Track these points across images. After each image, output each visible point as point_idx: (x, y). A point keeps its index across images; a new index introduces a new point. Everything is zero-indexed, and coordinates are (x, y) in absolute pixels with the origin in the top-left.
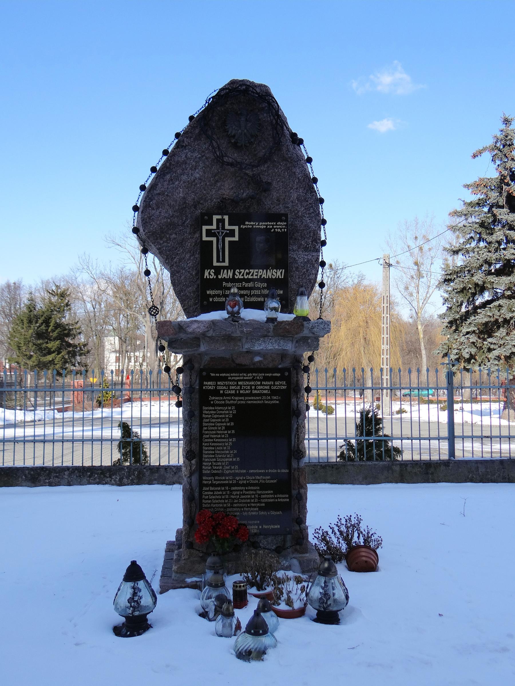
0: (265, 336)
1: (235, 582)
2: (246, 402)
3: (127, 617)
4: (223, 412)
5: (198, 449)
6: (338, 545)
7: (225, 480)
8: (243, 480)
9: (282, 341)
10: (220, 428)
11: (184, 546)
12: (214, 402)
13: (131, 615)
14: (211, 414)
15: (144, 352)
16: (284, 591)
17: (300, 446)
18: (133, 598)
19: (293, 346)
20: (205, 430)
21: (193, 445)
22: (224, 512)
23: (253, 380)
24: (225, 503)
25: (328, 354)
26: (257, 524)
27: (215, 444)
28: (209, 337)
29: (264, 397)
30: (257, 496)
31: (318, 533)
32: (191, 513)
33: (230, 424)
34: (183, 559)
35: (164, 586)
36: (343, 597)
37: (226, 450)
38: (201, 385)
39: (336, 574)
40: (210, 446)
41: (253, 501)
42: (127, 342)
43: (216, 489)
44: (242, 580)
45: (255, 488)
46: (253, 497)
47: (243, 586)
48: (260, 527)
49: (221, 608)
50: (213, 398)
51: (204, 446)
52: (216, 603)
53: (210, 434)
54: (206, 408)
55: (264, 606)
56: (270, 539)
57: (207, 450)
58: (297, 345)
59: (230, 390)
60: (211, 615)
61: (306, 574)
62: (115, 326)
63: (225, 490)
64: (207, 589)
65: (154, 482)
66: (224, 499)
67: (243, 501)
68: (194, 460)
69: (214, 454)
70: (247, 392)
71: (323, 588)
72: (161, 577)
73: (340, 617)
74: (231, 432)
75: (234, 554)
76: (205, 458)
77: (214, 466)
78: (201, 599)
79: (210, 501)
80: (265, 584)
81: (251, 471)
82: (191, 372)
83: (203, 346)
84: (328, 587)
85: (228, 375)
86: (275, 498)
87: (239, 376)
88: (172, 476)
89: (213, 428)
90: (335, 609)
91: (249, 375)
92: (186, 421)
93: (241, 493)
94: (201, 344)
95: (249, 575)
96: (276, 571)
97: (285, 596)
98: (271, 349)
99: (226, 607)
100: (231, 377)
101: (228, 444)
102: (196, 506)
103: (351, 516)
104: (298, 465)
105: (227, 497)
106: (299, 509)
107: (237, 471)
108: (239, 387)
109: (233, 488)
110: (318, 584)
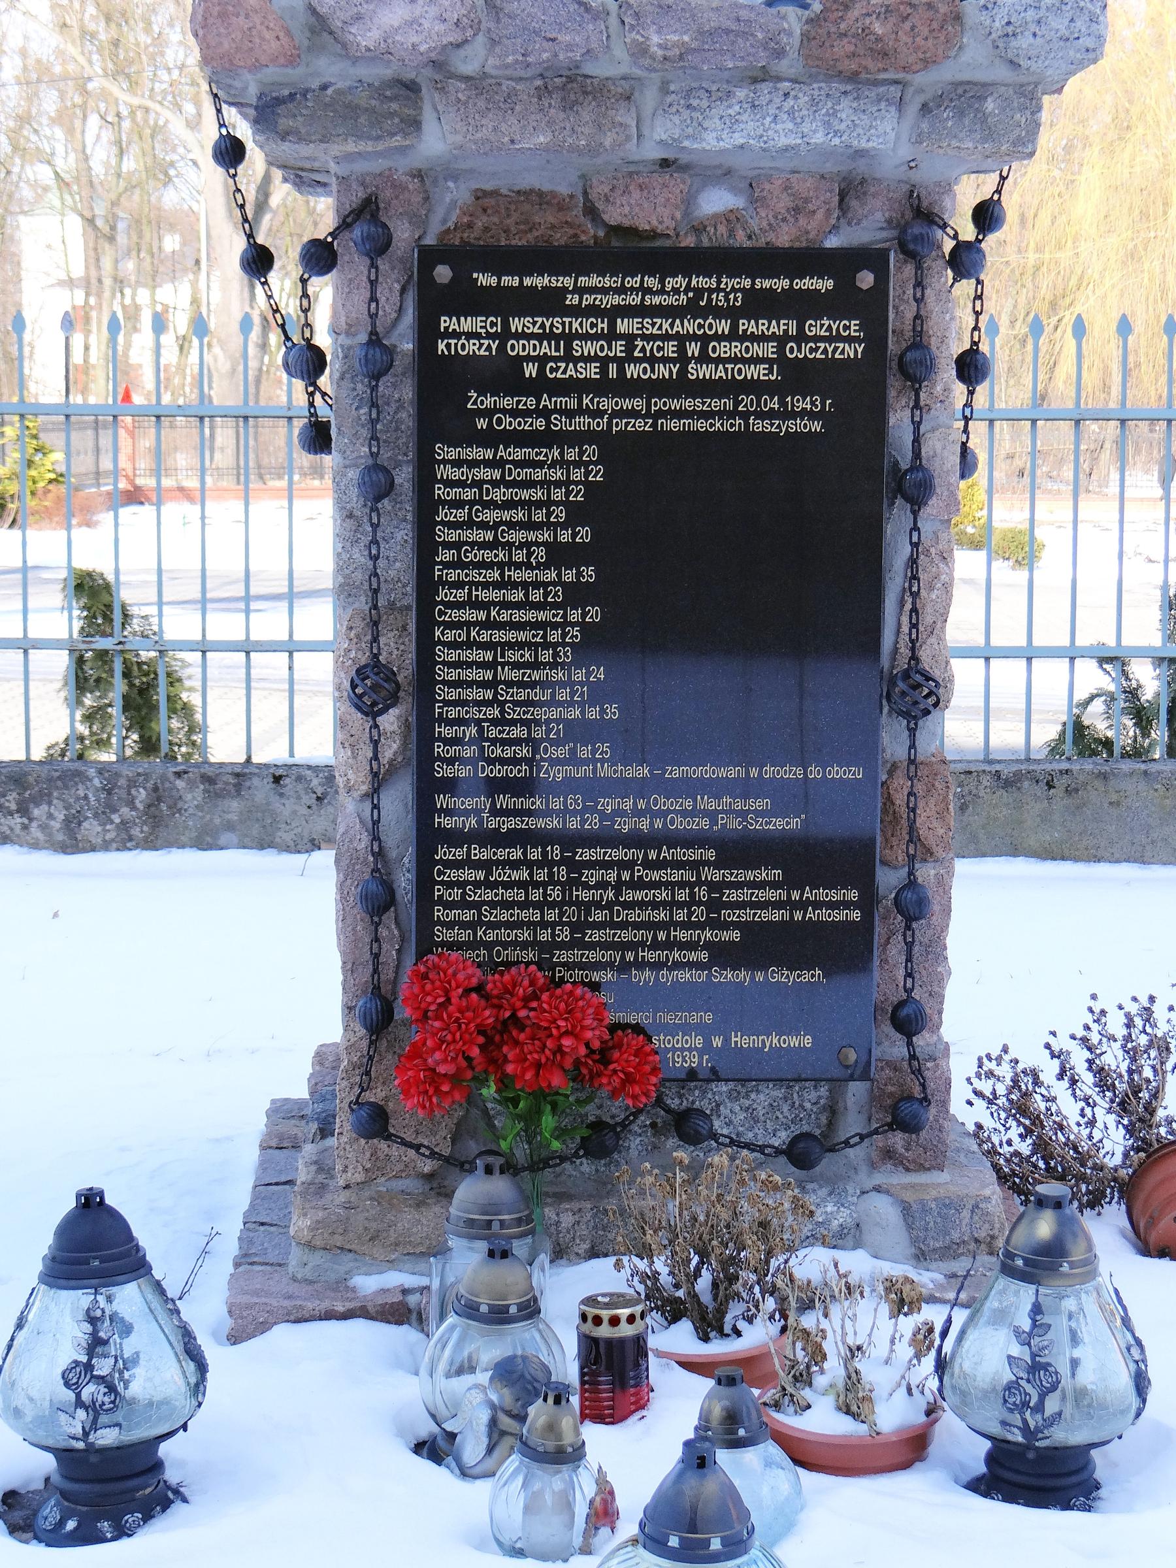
0: (759, 77)
1: (591, 1301)
2: (654, 425)
3: (63, 1455)
4: (539, 475)
5: (411, 656)
6: (1085, 1132)
7: (548, 813)
8: (638, 813)
9: (845, 103)
10: (519, 556)
11: (344, 1122)
12: (490, 424)
13: (81, 1445)
14: (478, 484)
15: (194, 284)
16: (828, 1346)
17: (924, 654)
18: (89, 1367)
19: (905, 137)
20: (447, 565)
21: (388, 640)
22: (540, 969)
23: (692, 310)
24: (544, 924)
25: (1022, 300)
26: (700, 1029)
27: (498, 636)
28: (467, 79)
29: (747, 402)
30: (702, 893)
31: (990, 1074)
32: (376, 971)
33: (574, 535)
34: (342, 1183)
35: (249, 1307)
36: (1123, 1380)
37: (554, 665)
38: (427, 332)
39: (1093, 1274)
40: (469, 644)
41: (680, 915)
42: (122, 239)
43: (501, 854)
44: (623, 1289)
45: (693, 855)
46: (682, 895)
47: (631, 1319)
48: (717, 1042)
49: (522, 1418)
50: (489, 401)
51: (444, 644)
52: (494, 1397)
53: (471, 583)
54: (453, 453)
55: (732, 1418)
56: (763, 1098)
57: (457, 665)
58: (925, 126)
59: (576, 360)
60: (472, 1449)
61: (934, 1265)
62: (66, 163)
63: (545, 862)
64: (452, 1328)
65: (224, 838)
66: (539, 905)
67: (634, 916)
68: (394, 712)
69: (492, 684)
70: (662, 371)
71: (1025, 1339)
72: (237, 1265)
73: (1099, 1474)
74: (579, 574)
75: (586, 1166)
76: (447, 703)
77: (494, 742)
78: (423, 1372)
79: (468, 915)
80: (735, 1310)
81: (675, 772)
82: (373, 265)
83: (435, 123)
84: (1049, 1336)
85: (568, 282)
86: (794, 906)
87: (621, 290)
88: (305, 811)
89: (488, 555)
90: (1077, 1437)
91: (670, 283)
92: (350, 516)
93: (626, 876)
94: (428, 117)
95: (661, 1265)
96: (791, 1249)
97: (834, 1368)
98: (786, 149)
99: (542, 1421)
100: (581, 291)
101: (564, 635)
102: (403, 939)
103: (1152, 999)
104: (913, 746)
105: (555, 894)
106: (909, 959)
107: (605, 771)
108: (618, 348)
109: (585, 854)
110: (1001, 1317)
